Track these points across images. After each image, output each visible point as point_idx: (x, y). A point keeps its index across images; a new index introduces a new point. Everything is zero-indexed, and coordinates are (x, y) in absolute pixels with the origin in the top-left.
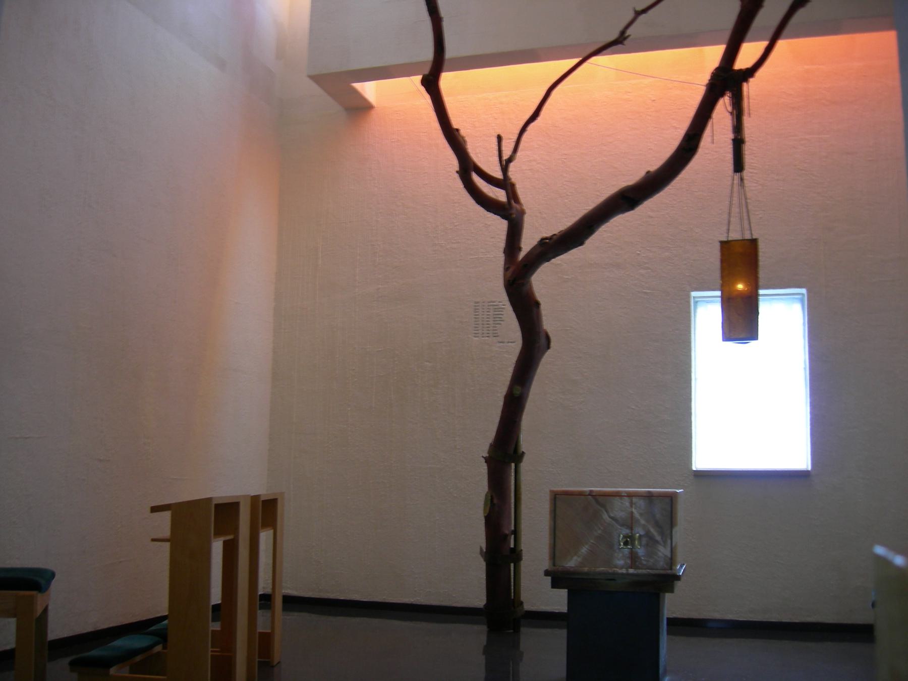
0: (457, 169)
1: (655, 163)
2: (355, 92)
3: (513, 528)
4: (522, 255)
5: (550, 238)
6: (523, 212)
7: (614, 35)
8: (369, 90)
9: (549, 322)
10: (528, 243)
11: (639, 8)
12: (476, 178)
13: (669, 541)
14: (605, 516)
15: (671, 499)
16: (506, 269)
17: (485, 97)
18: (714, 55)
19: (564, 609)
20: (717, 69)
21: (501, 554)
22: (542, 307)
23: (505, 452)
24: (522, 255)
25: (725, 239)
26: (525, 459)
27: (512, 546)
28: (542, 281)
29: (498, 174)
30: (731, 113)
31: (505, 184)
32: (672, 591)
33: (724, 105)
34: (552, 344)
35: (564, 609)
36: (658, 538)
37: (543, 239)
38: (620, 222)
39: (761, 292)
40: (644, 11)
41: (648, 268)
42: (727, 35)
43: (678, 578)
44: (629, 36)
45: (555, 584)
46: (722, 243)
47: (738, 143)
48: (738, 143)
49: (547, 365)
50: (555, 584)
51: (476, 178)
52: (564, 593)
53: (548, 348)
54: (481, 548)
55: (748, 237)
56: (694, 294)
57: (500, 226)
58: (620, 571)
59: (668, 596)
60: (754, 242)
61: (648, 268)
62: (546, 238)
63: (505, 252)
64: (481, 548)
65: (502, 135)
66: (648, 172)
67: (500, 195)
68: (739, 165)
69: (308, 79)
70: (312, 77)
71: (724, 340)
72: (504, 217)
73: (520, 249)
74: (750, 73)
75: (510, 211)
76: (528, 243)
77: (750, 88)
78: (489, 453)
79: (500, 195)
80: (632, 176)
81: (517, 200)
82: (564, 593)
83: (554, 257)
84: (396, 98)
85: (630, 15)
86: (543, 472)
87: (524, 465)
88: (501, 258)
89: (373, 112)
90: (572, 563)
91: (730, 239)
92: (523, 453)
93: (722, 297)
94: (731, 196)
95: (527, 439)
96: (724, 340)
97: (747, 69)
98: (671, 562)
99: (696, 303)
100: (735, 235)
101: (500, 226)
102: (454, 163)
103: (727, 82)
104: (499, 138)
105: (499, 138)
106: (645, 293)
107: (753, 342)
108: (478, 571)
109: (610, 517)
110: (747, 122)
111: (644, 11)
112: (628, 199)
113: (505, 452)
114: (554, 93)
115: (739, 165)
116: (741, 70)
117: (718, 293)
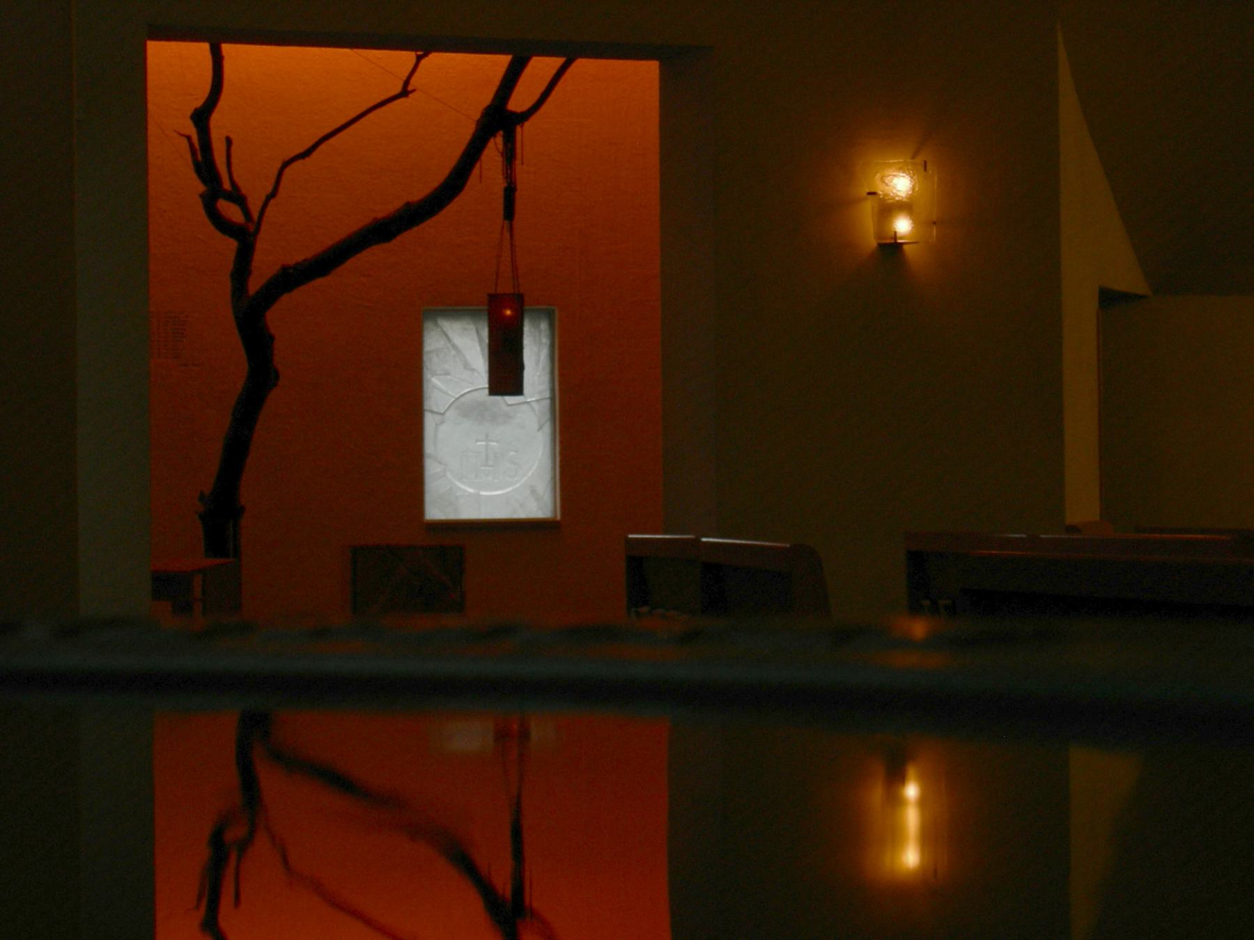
1: (419, 192)
9: (282, 355)
19: (153, 47)
20: (489, 107)
28: (277, 317)
33: (496, 144)
35: (153, 47)
46: (490, 296)
48: (510, 193)
49: (276, 400)
65: (233, 137)
66: (408, 204)
74: (519, 890)
75: (245, 237)
77: (525, 132)
92: (243, 508)
94: (502, 233)
95: (248, 493)
101: (232, 245)
103: (499, 120)
110: (520, 169)
112: (383, 230)
117: (486, 307)
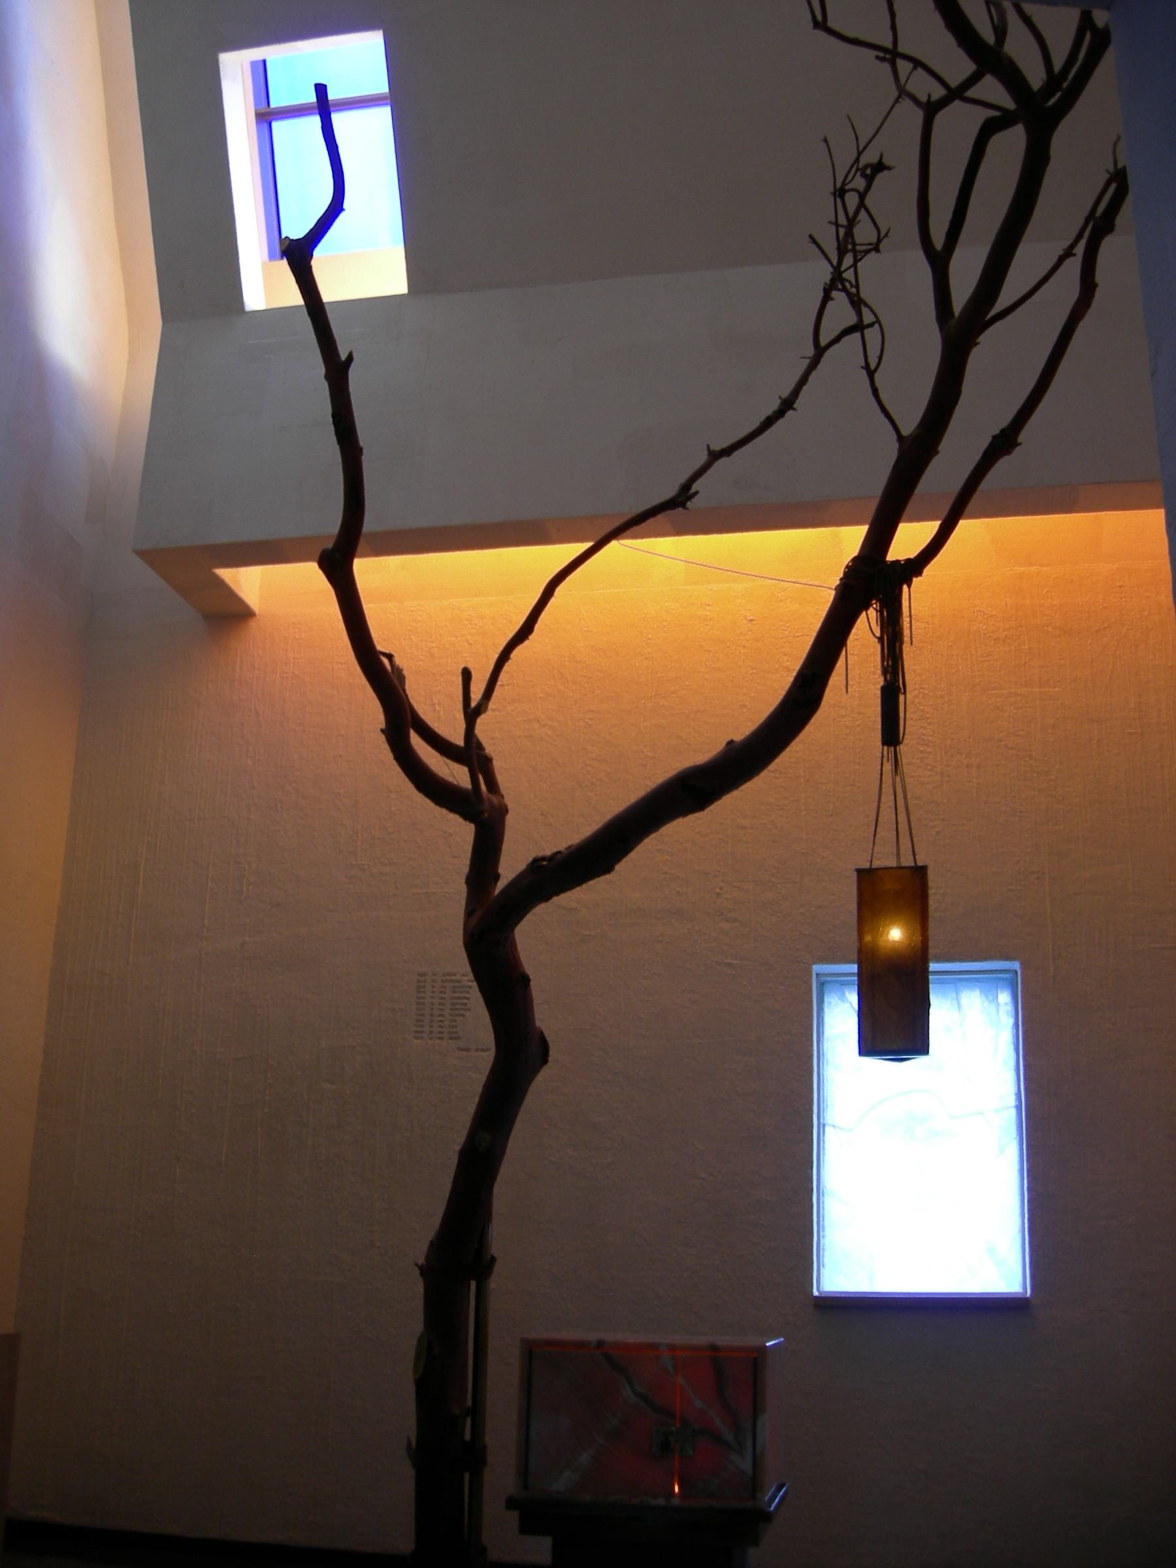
0: (383, 726)
2: (221, 584)
3: (469, 1403)
4: (501, 885)
5: (551, 859)
6: (504, 810)
7: (669, 491)
8: (250, 582)
10: (512, 864)
11: (717, 447)
12: (416, 740)
13: (749, 1444)
14: (627, 1392)
15: (756, 1359)
16: (469, 914)
17: (441, 600)
18: (851, 539)
20: (854, 560)
21: (445, 1448)
22: (533, 985)
23: (459, 1255)
24: (501, 885)
25: (866, 865)
26: (497, 1268)
27: (468, 1437)
28: (537, 937)
29: (457, 737)
30: (881, 639)
31: (471, 754)
32: (757, 1545)
34: (553, 1053)
36: (729, 1436)
37: (536, 860)
38: (679, 832)
39: (933, 966)
40: (727, 452)
41: (735, 920)
42: (872, 506)
43: (767, 1517)
44: (696, 493)
45: (528, 1526)
46: (860, 872)
47: (892, 693)
48: (892, 693)
49: (543, 1091)
50: (528, 1526)
51: (416, 740)
52: (546, 1542)
53: (545, 1061)
54: (409, 1442)
55: (907, 861)
56: (817, 968)
57: (463, 832)
58: (654, 1502)
59: (752, 1551)
60: (920, 872)
61: (735, 920)
62: (543, 859)
63: (467, 882)
64: (409, 1442)
65: (470, 666)
66: (730, 743)
67: (458, 775)
68: (891, 734)
69: (141, 567)
70: (143, 554)
71: (861, 1053)
72: (467, 817)
73: (497, 877)
75: (481, 809)
76: (512, 864)
77: (917, 597)
78: (427, 1258)
79: (458, 775)
80: (703, 749)
81: (493, 785)
82: (546, 1542)
83: (557, 894)
84: (283, 592)
85: (703, 458)
86: (533, 1291)
87: (495, 1283)
88: (459, 890)
89: (252, 624)
90: (561, 1483)
91: (877, 864)
93: (860, 974)
96: (861, 1053)
97: (908, 561)
98: (755, 1484)
99: (822, 986)
100: (884, 860)
101: (463, 832)
102: (373, 713)
103: (874, 583)
104: (467, 675)
105: (467, 675)
106: (730, 965)
107: (918, 1062)
108: (401, 1481)
109: (635, 1392)
111: (727, 452)
112: (694, 790)
113: (459, 1255)
114: (560, 590)
115: (891, 734)
116: (898, 562)
117: (854, 968)
